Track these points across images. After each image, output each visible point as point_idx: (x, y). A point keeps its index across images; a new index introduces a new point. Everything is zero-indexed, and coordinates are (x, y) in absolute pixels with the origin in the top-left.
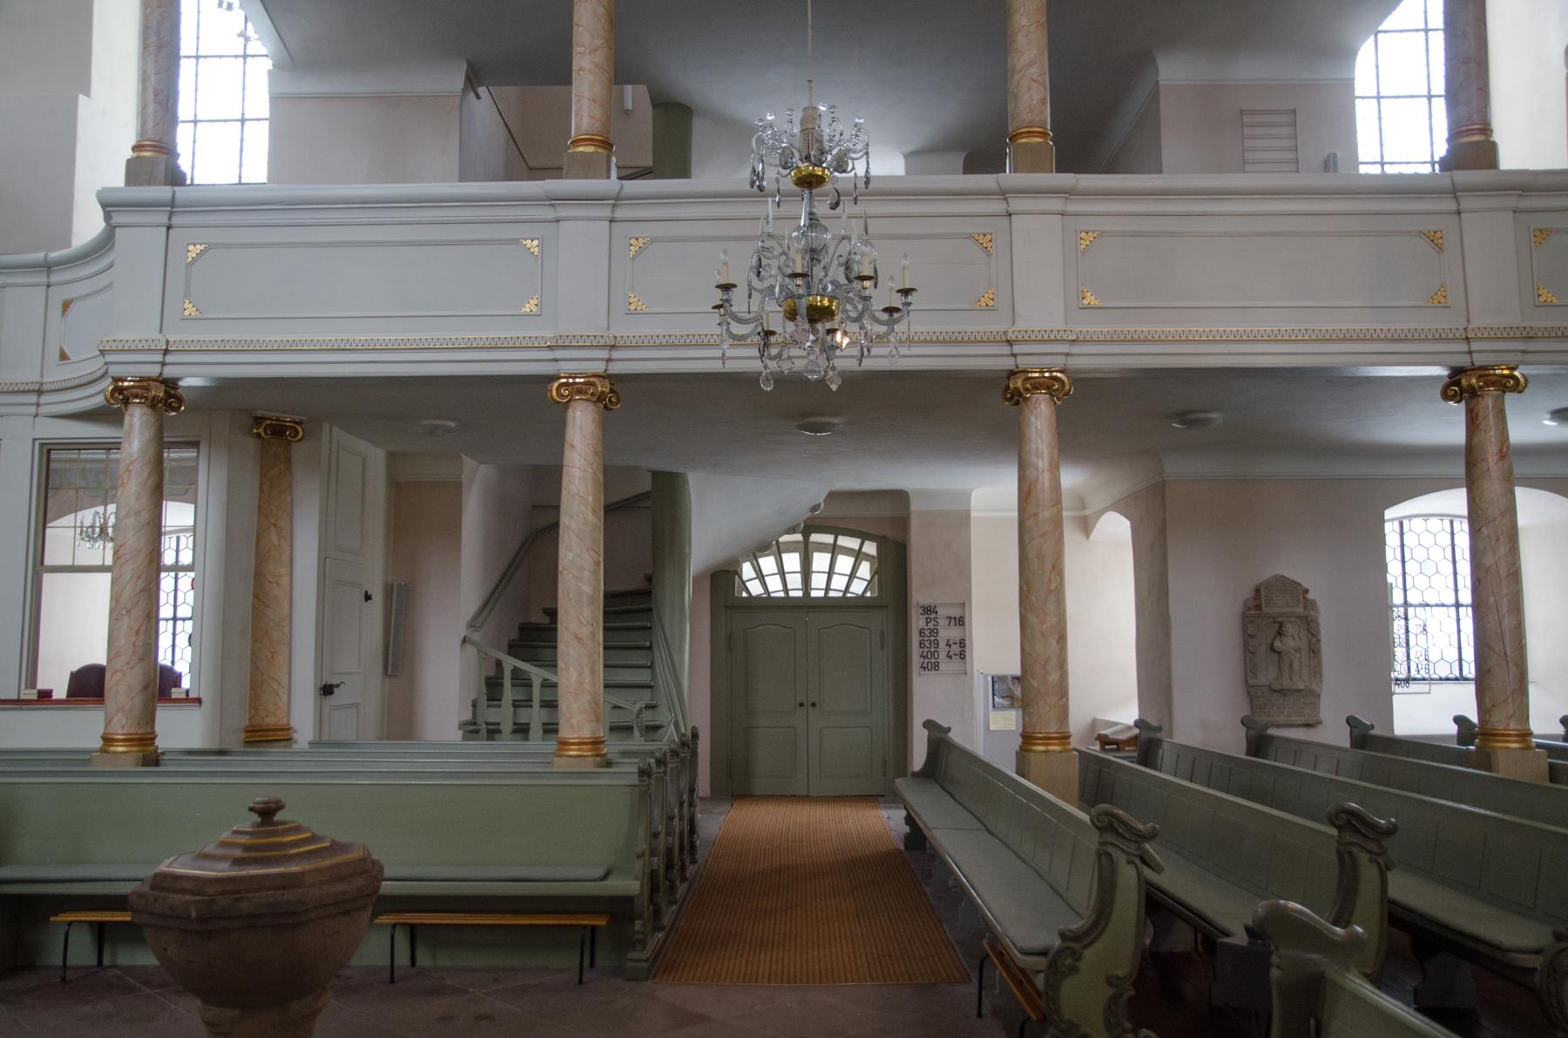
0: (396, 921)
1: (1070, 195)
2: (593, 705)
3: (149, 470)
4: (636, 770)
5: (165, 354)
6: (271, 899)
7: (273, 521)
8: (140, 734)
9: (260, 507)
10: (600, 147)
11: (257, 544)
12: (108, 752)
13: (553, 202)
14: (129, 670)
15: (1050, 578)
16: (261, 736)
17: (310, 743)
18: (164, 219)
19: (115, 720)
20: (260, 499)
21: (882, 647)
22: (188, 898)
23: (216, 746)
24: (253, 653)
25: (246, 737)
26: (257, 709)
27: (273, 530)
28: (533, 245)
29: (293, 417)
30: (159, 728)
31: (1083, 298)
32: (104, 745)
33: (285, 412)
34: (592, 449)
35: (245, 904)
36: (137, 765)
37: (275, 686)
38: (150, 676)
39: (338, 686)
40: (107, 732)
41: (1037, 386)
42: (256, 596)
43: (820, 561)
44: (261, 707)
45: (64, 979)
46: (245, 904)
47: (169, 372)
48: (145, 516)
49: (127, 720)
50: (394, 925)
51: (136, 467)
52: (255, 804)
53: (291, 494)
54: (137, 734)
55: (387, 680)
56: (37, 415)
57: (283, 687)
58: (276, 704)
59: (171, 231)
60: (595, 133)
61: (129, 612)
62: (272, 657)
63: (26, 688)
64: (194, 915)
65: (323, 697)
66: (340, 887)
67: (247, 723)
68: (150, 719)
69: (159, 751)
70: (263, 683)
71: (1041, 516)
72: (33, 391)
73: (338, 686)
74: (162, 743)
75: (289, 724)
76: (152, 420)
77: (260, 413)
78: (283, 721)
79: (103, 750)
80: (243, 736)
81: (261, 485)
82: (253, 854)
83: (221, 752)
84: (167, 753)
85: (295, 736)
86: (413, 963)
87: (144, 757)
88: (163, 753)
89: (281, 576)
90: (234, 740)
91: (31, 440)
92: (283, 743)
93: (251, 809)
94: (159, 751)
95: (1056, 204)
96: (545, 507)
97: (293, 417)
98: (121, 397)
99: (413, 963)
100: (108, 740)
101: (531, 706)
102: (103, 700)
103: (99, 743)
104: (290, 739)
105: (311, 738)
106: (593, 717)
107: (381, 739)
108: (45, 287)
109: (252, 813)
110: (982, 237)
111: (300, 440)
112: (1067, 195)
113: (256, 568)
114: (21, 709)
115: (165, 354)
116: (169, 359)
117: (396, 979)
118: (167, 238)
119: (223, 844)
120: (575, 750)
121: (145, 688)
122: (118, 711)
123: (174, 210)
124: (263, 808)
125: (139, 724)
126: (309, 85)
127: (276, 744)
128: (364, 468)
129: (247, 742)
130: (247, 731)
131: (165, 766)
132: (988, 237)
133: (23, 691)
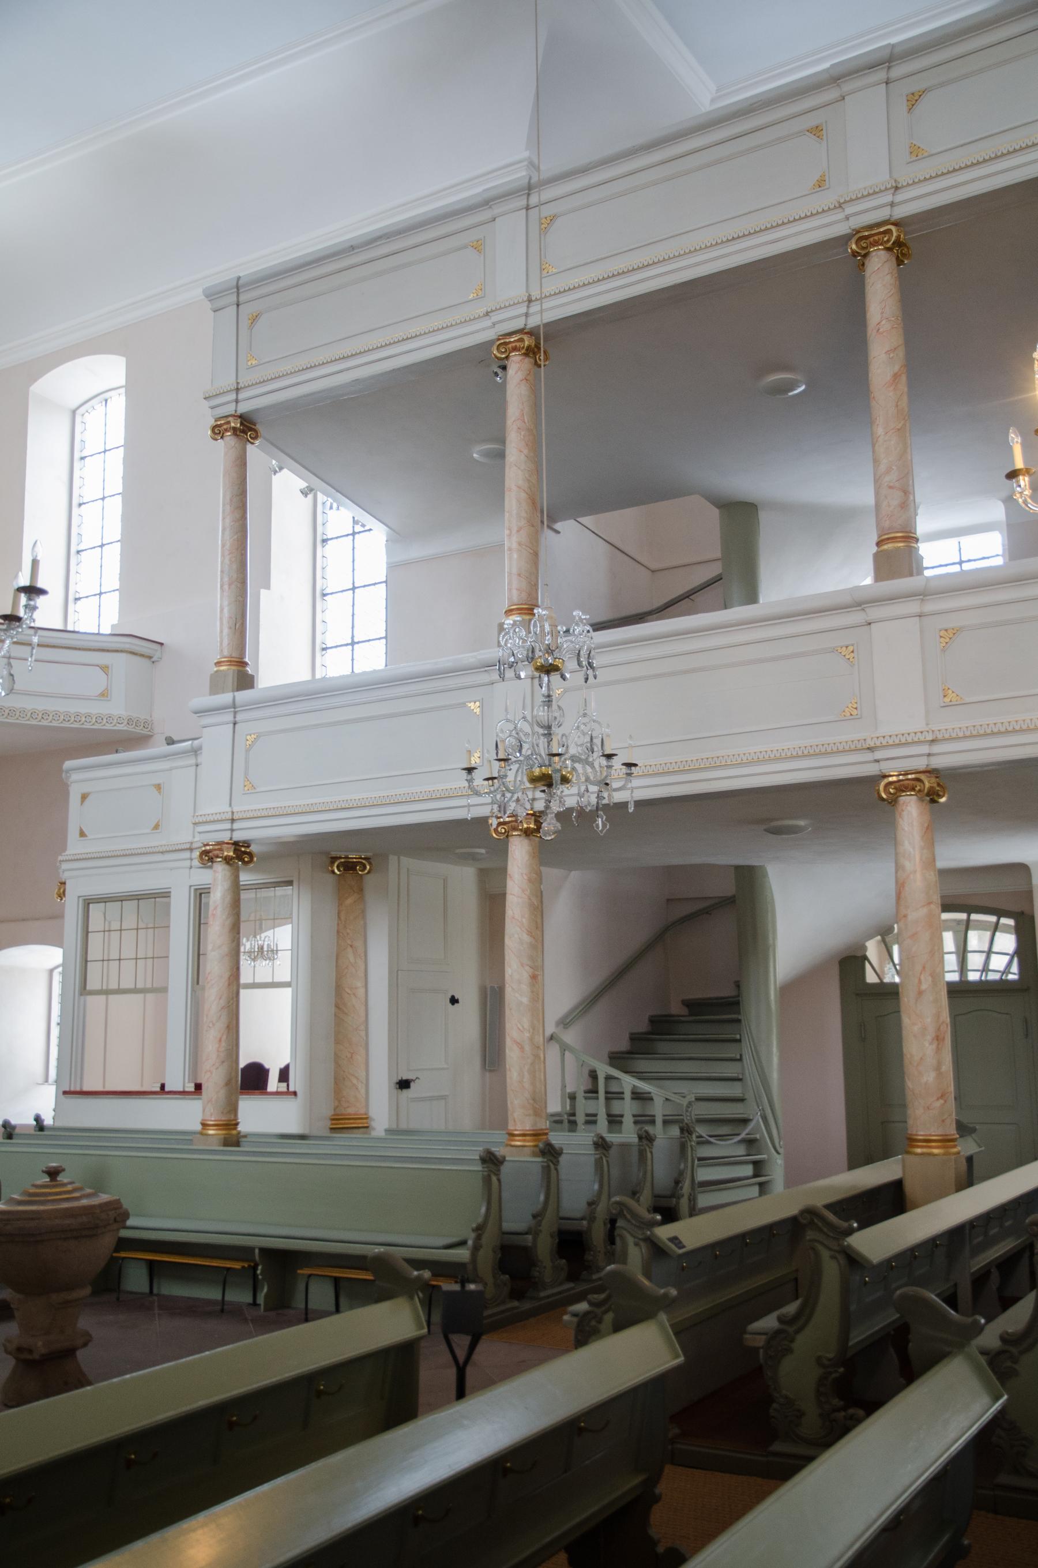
1: (924, 596)
2: (531, 1102)
3: (227, 913)
4: (478, 1158)
5: (232, 823)
7: (349, 942)
8: (224, 1121)
9: (338, 932)
10: (525, 614)
11: (337, 962)
13: (487, 668)
15: (920, 980)
17: (386, 1130)
18: (229, 717)
20: (338, 924)
21: (1027, 1036)
24: (335, 1054)
27: (349, 950)
28: (475, 707)
29: (360, 854)
30: (242, 1116)
31: (945, 696)
33: (341, 851)
34: (526, 877)
37: (355, 1081)
41: (902, 788)
42: (337, 1006)
43: (976, 940)
44: (343, 1099)
45: (118, 1299)
47: (238, 836)
48: (225, 949)
51: (219, 910)
53: (364, 917)
54: (221, 1121)
55: (488, 1074)
56: (191, 867)
57: (362, 1083)
59: (237, 726)
60: (524, 602)
61: (213, 1025)
62: (352, 1057)
63: (189, 1082)
65: (400, 1091)
66: (67, 1222)
67: (333, 1113)
68: (233, 1109)
70: (344, 1079)
71: (910, 918)
72: (187, 849)
74: (246, 1126)
76: (228, 874)
77: (334, 854)
78: (362, 1111)
80: (328, 1124)
81: (339, 913)
82: (30, 1199)
85: (374, 1124)
89: (356, 988)
90: (321, 1127)
91: (188, 888)
95: (913, 607)
96: (680, 899)
97: (360, 854)
98: (207, 858)
100: (204, 1125)
101: (623, 1099)
103: (199, 1127)
105: (385, 1125)
106: (531, 1112)
108: (195, 767)
110: (844, 648)
111: (369, 872)
112: (921, 597)
113: (337, 982)
115: (232, 823)
116: (236, 826)
118: (234, 732)
120: (519, 1141)
123: (236, 710)
126: (416, 551)
127: (344, 1130)
128: (445, 887)
129: (331, 1129)
132: (851, 648)
133: (187, 1085)
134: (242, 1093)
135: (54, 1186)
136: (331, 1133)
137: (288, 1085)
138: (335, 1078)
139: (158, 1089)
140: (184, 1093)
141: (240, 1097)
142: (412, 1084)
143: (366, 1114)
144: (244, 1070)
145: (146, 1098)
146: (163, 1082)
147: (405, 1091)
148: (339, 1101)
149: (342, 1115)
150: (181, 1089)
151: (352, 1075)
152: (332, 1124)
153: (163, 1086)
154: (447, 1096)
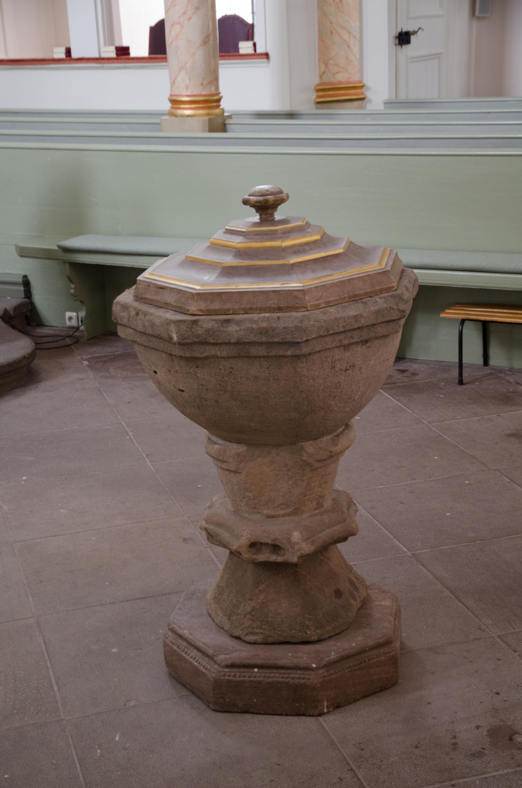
0: (465, 317)
6: (264, 325)
8: (205, 96)
12: (176, 116)
14: (186, 22)
16: (329, 96)
19: (179, 79)
22: (171, 316)
23: (286, 108)
25: (318, 97)
26: (326, 65)
32: (172, 108)
35: (232, 328)
36: (204, 131)
37: (346, 36)
38: (208, 29)
39: (415, 33)
40: (173, 93)
44: (331, 62)
46: (232, 328)
49: (189, 80)
50: (463, 321)
52: (250, 195)
54: (200, 95)
55: (475, 23)
57: (354, 37)
58: (347, 58)
63: (105, 45)
64: (175, 338)
65: (399, 47)
67: (317, 81)
69: (226, 114)
73: (415, 33)
75: (361, 82)
78: (355, 78)
79: (172, 114)
80: (313, 95)
82: (246, 263)
83: (291, 115)
84: (233, 116)
85: (369, 94)
86: (486, 363)
87: (210, 121)
88: (230, 117)
92: (356, 103)
93: (246, 202)
94: (226, 114)
99: (486, 363)
100: (175, 102)
102: (166, 58)
103: (167, 106)
104: (363, 99)
105: (385, 96)
107: (468, 96)
109: (248, 207)
114: (103, 68)
117: (464, 381)
119: (216, 247)
121: (205, 42)
122: (180, 70)
124: (260, 202)
125: (202, 84)
127: (336, 105)
129: (318, 103)
130: (318, 91)
131: (232, 131)
133: (103, 49)
134: (222, 57)
135: (272, 235)
136: (317, 108)
137: (255, 45)
138: (320, 31)
139: (63, 56)
140: (100, 60)
141: (220, 62)
142: (413, 38)
143: (361, 82)
144: (220, 20)
145: (45, 69)
146: (68, 46)
147: (405, 47)
148: (326, 65)
149: (329, 83)
150: (96, 55)
151: (343, 28)
152: (318, 97)
153: (68, 52)
154: (441, 54)
